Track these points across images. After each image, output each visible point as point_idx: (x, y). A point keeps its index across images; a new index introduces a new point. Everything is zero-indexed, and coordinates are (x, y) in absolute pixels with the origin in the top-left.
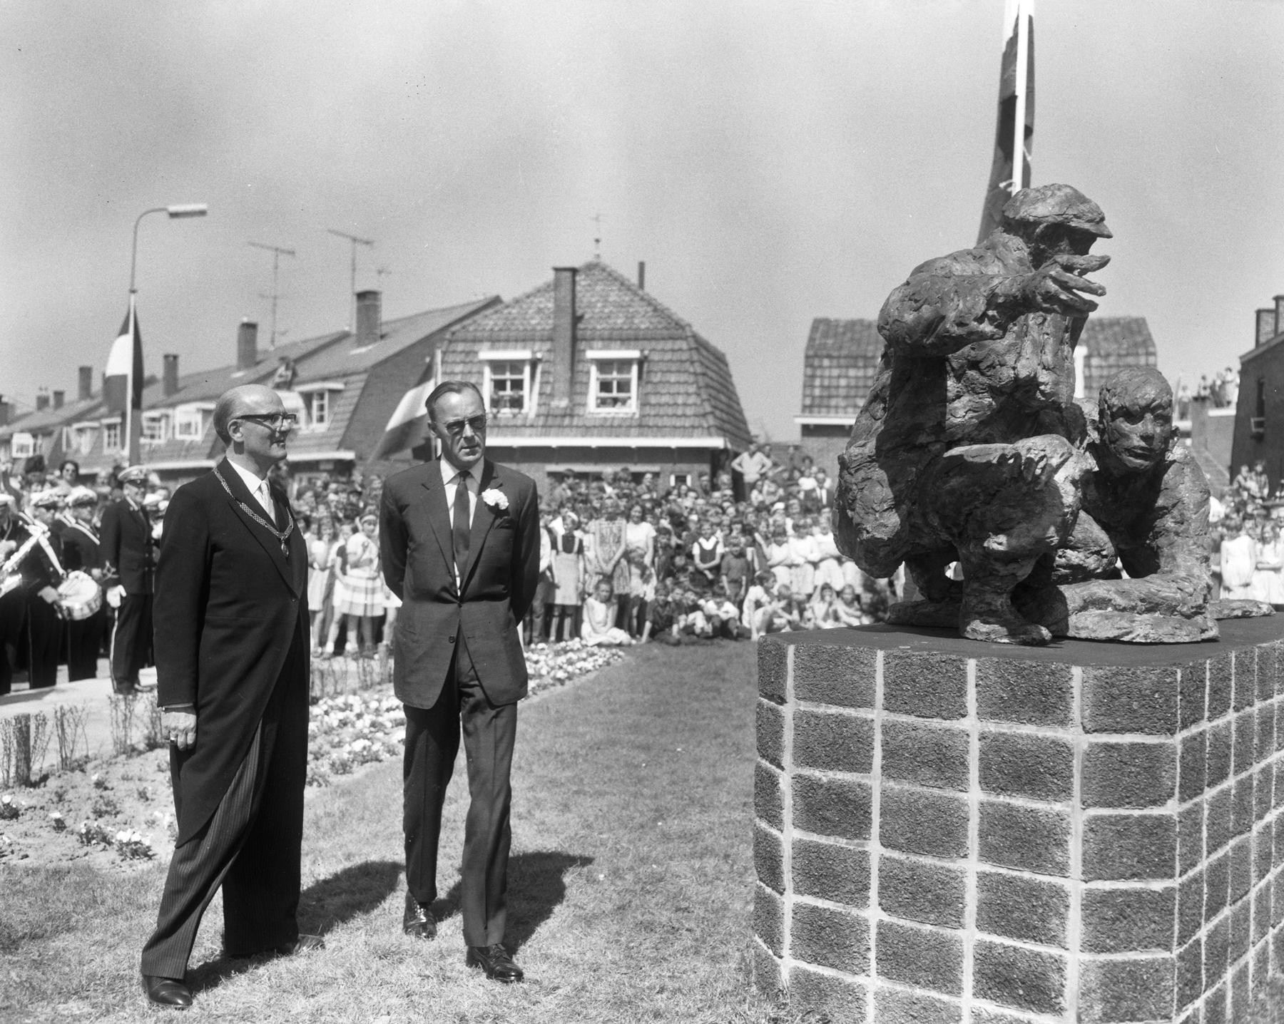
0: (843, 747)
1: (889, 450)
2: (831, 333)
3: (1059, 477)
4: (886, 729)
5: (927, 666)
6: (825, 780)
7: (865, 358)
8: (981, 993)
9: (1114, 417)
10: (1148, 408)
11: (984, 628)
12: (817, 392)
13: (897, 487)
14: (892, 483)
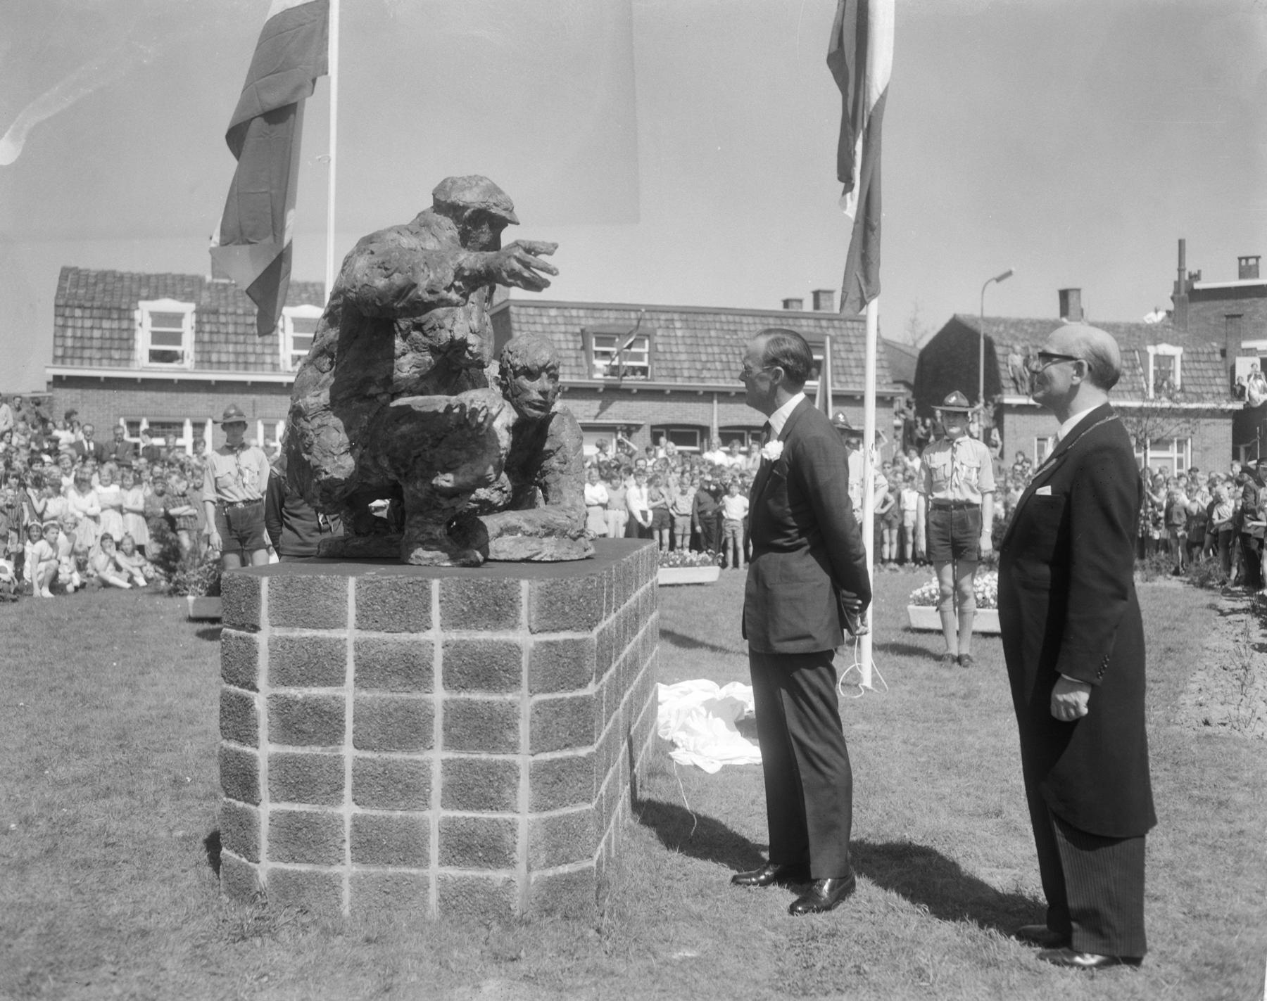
0: (318, 665)
1: (343, 400)
2: (82, 283)
3: (497, 424)
4: (358, 646)
5: (396, 587)
6: (300, 696)
7: (119, 309)
8: (446, 861)
9: (516, 375)
10: (544, 368)
11: (428, 554)
12: (69, 342)
13: (353, 432)
14: (348, 429)
